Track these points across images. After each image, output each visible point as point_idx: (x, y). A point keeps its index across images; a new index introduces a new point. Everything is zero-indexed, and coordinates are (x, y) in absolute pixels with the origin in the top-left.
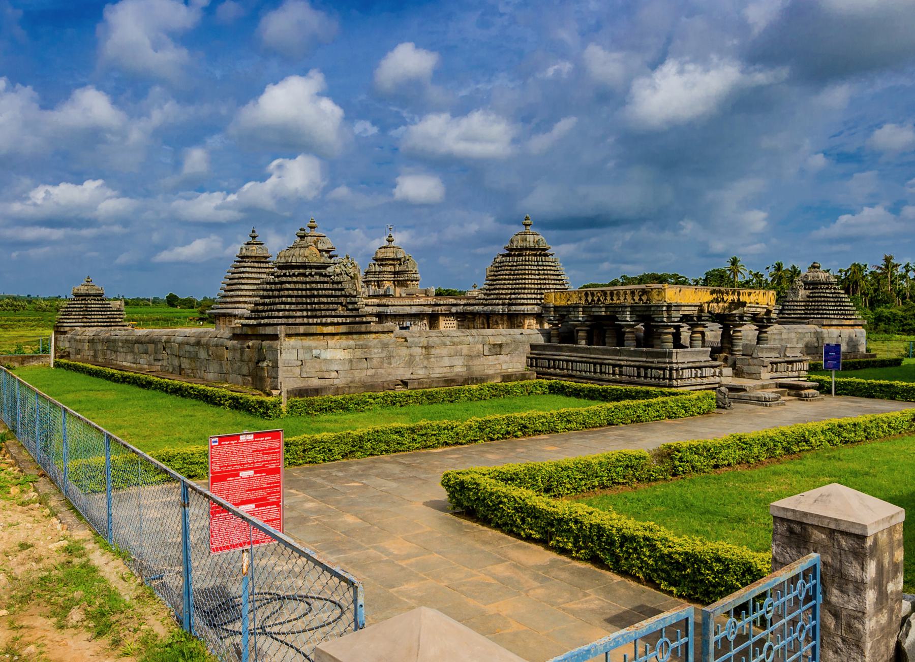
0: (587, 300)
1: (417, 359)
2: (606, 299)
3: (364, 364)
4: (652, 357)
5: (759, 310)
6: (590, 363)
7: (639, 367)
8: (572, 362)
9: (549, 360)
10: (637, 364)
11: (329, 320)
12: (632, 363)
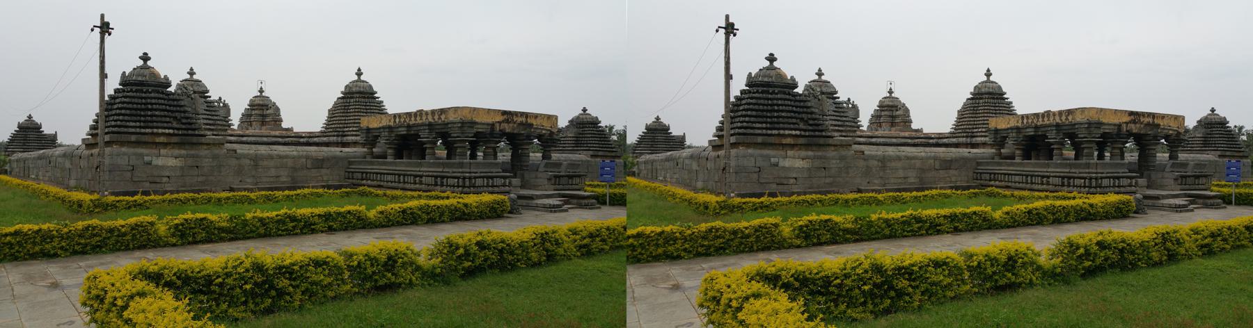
11: (160, 131)
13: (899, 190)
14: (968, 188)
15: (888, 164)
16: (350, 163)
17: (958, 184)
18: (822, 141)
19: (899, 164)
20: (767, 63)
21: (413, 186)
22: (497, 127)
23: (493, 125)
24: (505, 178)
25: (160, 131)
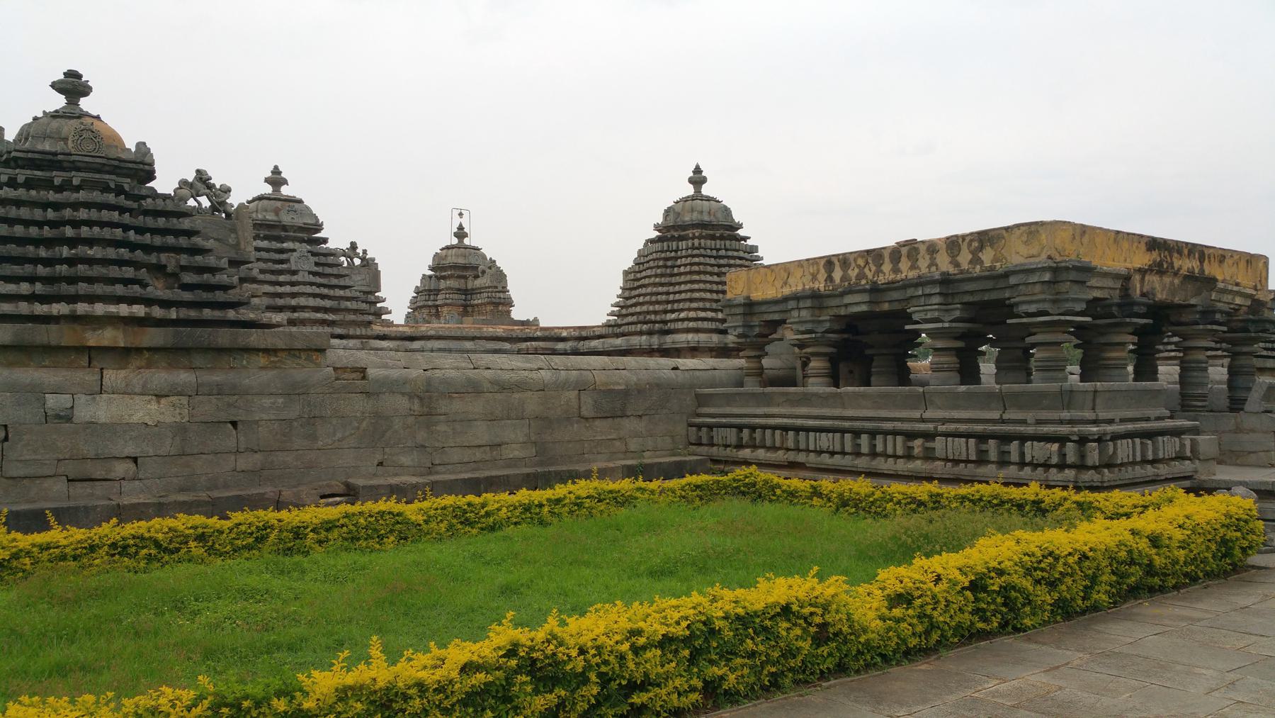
0: (830, 278)
1: (397, 424)
2: (879, 271)
3: (230, 439)
4: (1020, 407)
5: (1238, 301)
6: (843, 431)
7: (982, 438)
8: (797, 430)
9: (740, 428)
10: (979, 428)
11: (100, 309)
12: (963, 427)
13: (476, 486)
14: (677, 470)
15: (443, 406)
16: (702, 400)
17: (648, 459)
18: (223, 337)
19: (476, 407)
20: (58, 101)
21: (902, 466)
22: (1137, 288)
23: (1127, 278)
24: (1177, 433)
25: (100, 309)
